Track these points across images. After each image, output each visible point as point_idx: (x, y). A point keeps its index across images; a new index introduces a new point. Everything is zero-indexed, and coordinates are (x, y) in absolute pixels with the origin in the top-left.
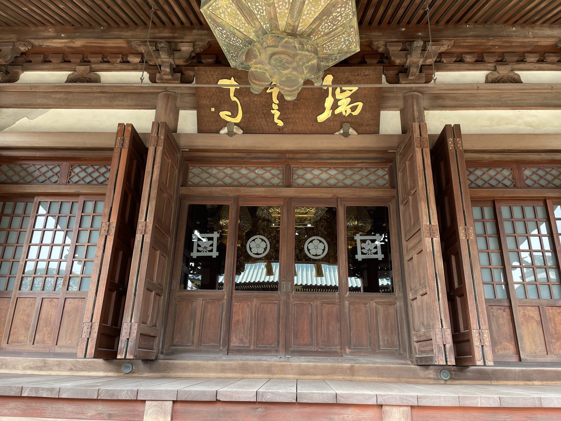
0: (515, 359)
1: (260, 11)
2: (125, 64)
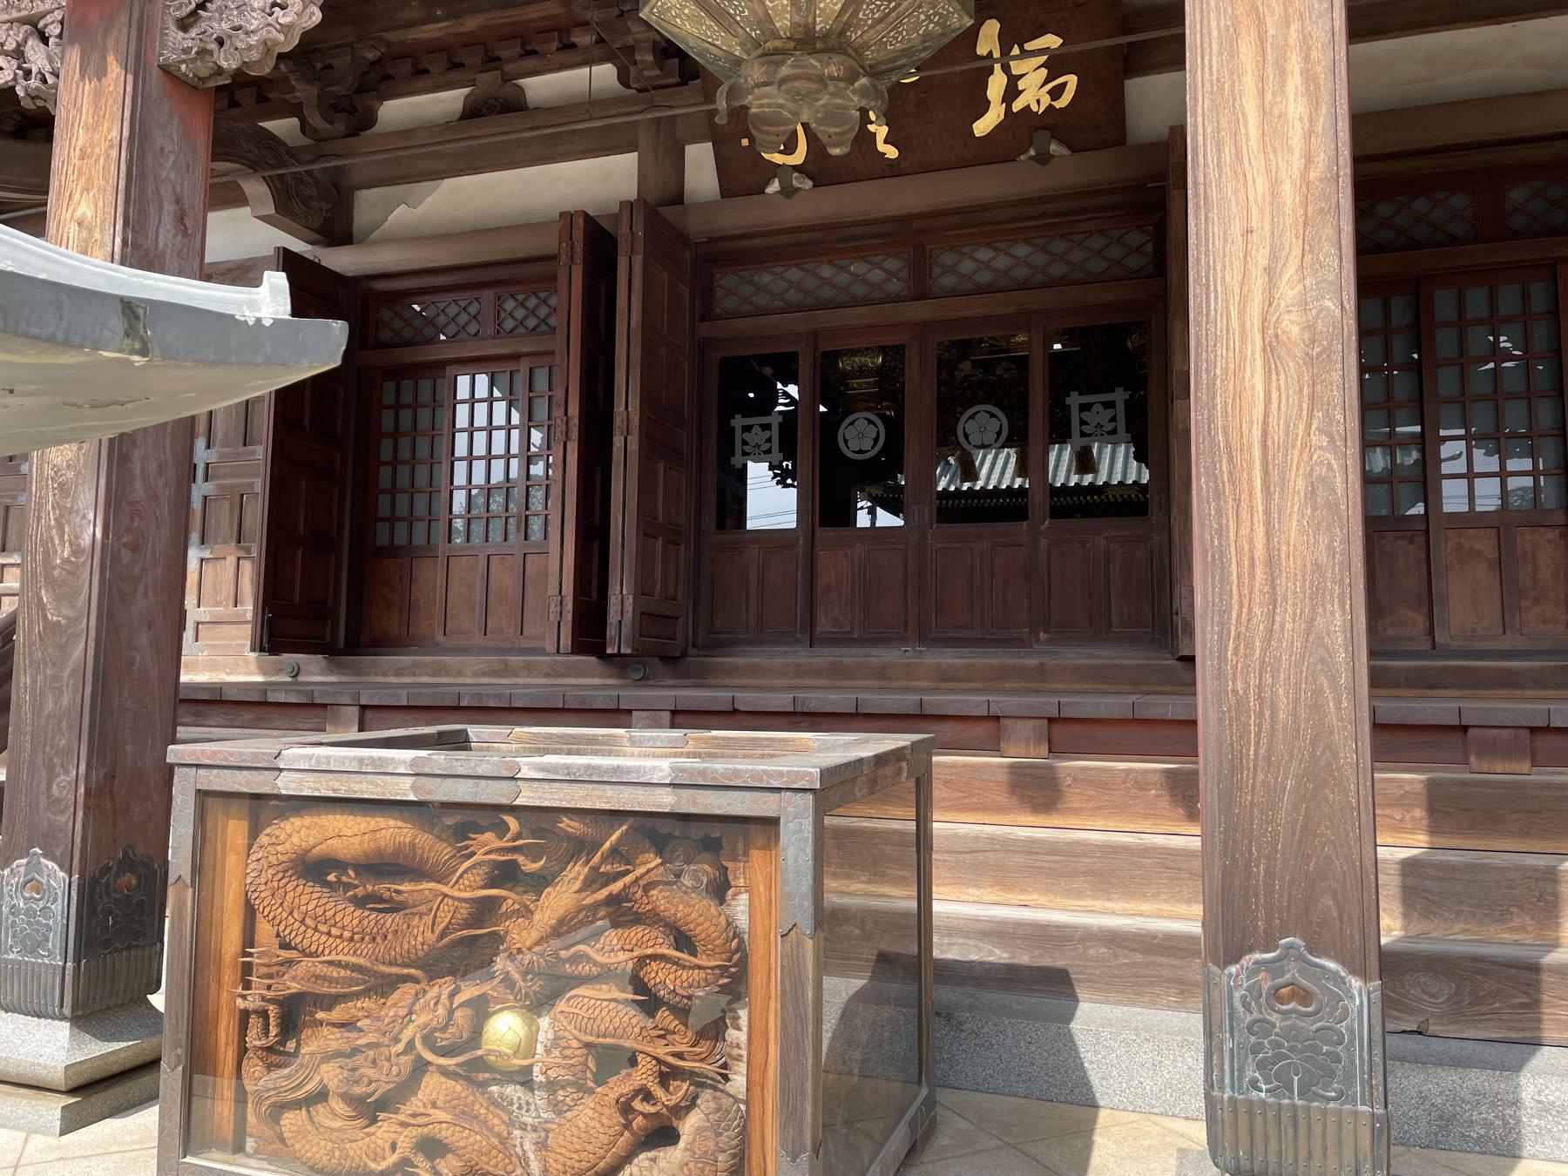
0: (1425, 645)
1: (741, 11)
2: (570, 55)
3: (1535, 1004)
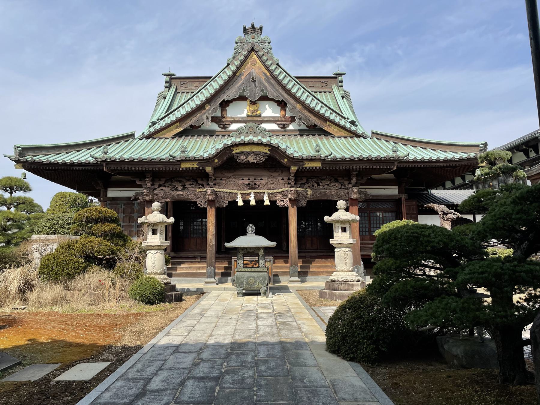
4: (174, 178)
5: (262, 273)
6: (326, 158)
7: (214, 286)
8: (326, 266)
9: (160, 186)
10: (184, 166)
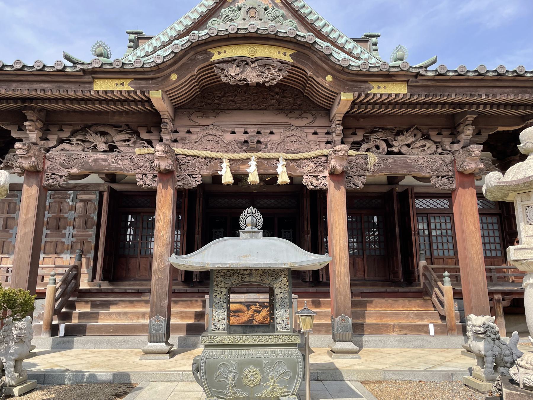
3: (363, 329)
4: (89, 127)
5: (284, 351)
6: (422, 71)
7: (164, 361)
8: (396, 314)
9: (61, 141)
10: (101, 86)
